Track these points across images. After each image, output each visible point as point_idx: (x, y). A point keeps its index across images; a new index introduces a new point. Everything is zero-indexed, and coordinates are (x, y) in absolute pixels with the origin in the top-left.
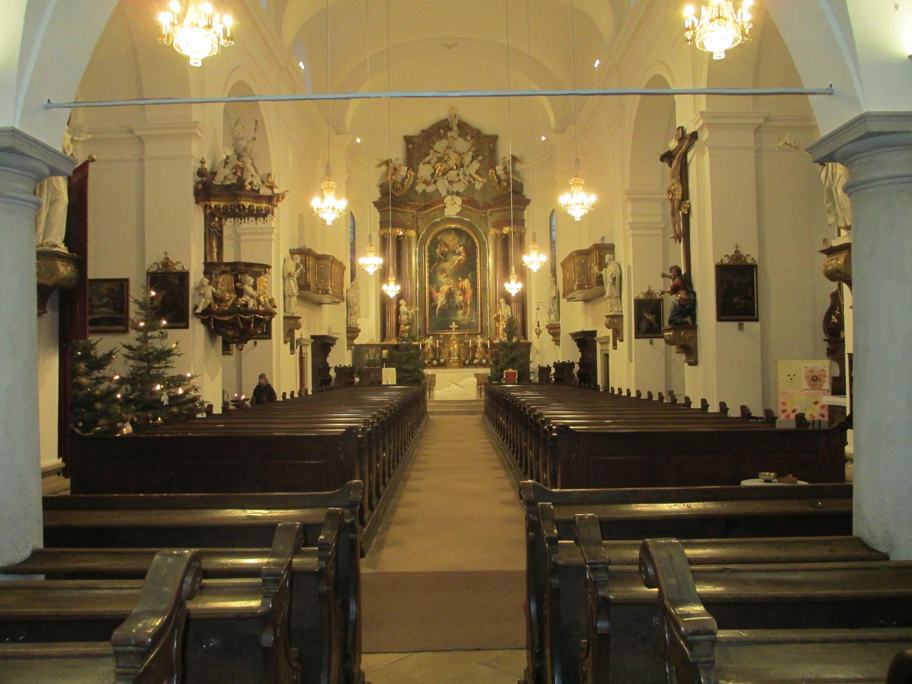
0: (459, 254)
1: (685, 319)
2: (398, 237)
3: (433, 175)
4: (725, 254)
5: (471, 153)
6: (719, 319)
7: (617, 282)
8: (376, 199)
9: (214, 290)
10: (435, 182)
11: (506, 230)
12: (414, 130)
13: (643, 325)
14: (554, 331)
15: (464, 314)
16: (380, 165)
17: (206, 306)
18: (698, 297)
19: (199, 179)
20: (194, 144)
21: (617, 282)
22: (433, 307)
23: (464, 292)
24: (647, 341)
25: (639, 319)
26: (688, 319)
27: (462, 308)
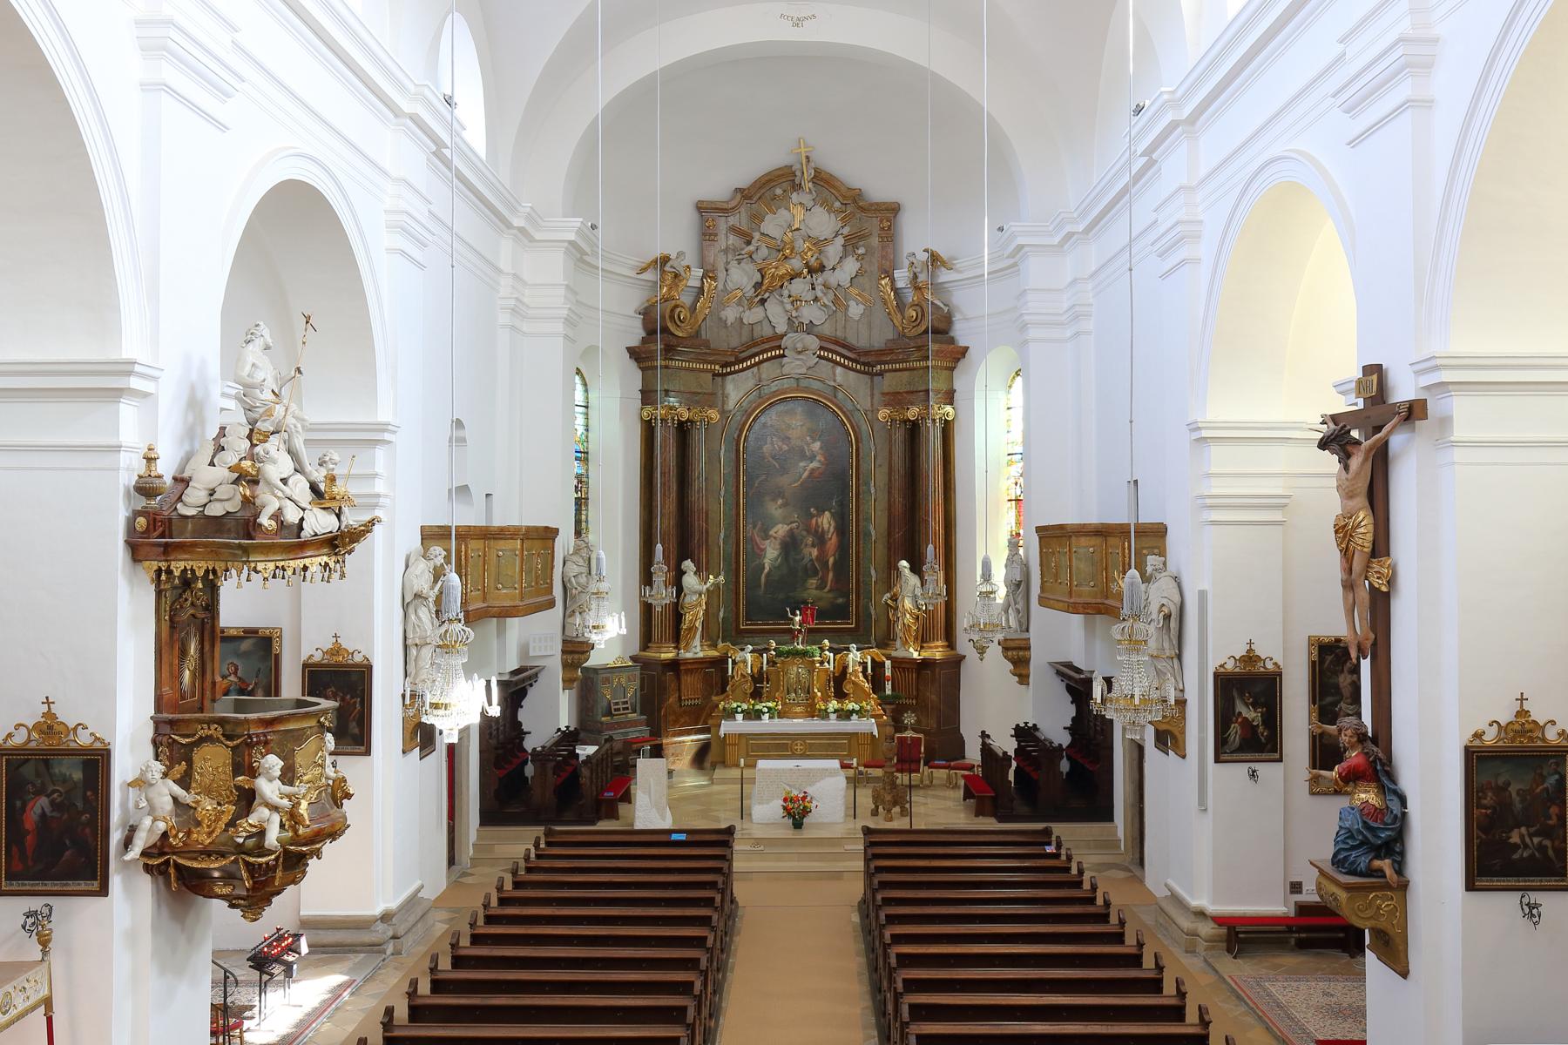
0: (812, 458)
1: (1377, 863)
2: (681, 424)
3: (758, 286)
4: (1488, 714)
5: (840, 241)
6: (1470, 886)
7: (1173, 624)
8: (635, 341)
9: (179, 791)
10: (763, 302)
11: (913, 413)
12: (718, 187)
13: (1235, 730)
14: (1018, 655)
15: (821, 587)
16: (644, 270)
17: (155, 838)
18: (1413, 808)
19: (141, 503)
20: (127, 411)
21: (1173, 624)
22: (753, 583)
23: (820, 539)
24: (1242, 769)
25: (1224, 717)
26: (1385, 865)
27: (815, 573)
